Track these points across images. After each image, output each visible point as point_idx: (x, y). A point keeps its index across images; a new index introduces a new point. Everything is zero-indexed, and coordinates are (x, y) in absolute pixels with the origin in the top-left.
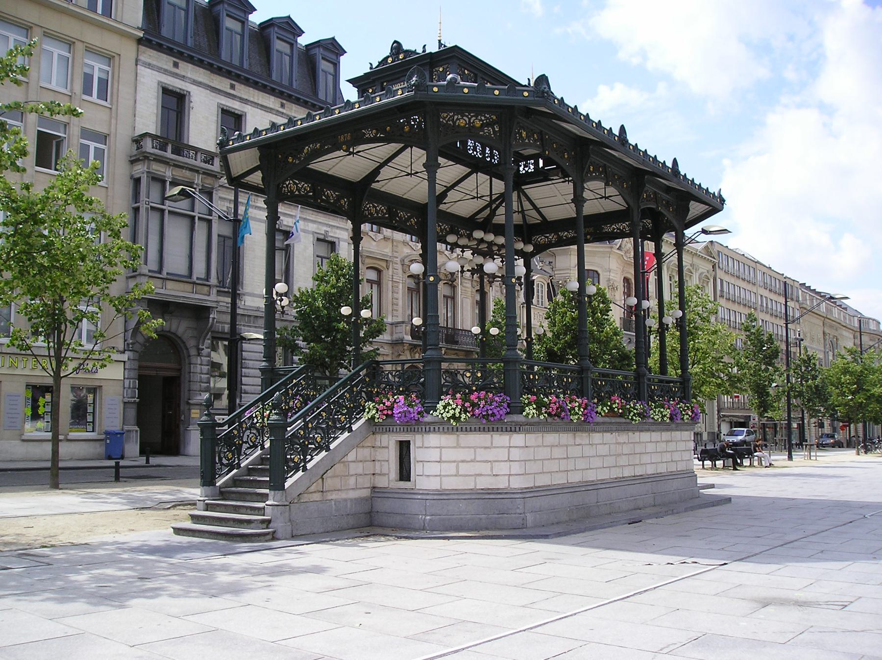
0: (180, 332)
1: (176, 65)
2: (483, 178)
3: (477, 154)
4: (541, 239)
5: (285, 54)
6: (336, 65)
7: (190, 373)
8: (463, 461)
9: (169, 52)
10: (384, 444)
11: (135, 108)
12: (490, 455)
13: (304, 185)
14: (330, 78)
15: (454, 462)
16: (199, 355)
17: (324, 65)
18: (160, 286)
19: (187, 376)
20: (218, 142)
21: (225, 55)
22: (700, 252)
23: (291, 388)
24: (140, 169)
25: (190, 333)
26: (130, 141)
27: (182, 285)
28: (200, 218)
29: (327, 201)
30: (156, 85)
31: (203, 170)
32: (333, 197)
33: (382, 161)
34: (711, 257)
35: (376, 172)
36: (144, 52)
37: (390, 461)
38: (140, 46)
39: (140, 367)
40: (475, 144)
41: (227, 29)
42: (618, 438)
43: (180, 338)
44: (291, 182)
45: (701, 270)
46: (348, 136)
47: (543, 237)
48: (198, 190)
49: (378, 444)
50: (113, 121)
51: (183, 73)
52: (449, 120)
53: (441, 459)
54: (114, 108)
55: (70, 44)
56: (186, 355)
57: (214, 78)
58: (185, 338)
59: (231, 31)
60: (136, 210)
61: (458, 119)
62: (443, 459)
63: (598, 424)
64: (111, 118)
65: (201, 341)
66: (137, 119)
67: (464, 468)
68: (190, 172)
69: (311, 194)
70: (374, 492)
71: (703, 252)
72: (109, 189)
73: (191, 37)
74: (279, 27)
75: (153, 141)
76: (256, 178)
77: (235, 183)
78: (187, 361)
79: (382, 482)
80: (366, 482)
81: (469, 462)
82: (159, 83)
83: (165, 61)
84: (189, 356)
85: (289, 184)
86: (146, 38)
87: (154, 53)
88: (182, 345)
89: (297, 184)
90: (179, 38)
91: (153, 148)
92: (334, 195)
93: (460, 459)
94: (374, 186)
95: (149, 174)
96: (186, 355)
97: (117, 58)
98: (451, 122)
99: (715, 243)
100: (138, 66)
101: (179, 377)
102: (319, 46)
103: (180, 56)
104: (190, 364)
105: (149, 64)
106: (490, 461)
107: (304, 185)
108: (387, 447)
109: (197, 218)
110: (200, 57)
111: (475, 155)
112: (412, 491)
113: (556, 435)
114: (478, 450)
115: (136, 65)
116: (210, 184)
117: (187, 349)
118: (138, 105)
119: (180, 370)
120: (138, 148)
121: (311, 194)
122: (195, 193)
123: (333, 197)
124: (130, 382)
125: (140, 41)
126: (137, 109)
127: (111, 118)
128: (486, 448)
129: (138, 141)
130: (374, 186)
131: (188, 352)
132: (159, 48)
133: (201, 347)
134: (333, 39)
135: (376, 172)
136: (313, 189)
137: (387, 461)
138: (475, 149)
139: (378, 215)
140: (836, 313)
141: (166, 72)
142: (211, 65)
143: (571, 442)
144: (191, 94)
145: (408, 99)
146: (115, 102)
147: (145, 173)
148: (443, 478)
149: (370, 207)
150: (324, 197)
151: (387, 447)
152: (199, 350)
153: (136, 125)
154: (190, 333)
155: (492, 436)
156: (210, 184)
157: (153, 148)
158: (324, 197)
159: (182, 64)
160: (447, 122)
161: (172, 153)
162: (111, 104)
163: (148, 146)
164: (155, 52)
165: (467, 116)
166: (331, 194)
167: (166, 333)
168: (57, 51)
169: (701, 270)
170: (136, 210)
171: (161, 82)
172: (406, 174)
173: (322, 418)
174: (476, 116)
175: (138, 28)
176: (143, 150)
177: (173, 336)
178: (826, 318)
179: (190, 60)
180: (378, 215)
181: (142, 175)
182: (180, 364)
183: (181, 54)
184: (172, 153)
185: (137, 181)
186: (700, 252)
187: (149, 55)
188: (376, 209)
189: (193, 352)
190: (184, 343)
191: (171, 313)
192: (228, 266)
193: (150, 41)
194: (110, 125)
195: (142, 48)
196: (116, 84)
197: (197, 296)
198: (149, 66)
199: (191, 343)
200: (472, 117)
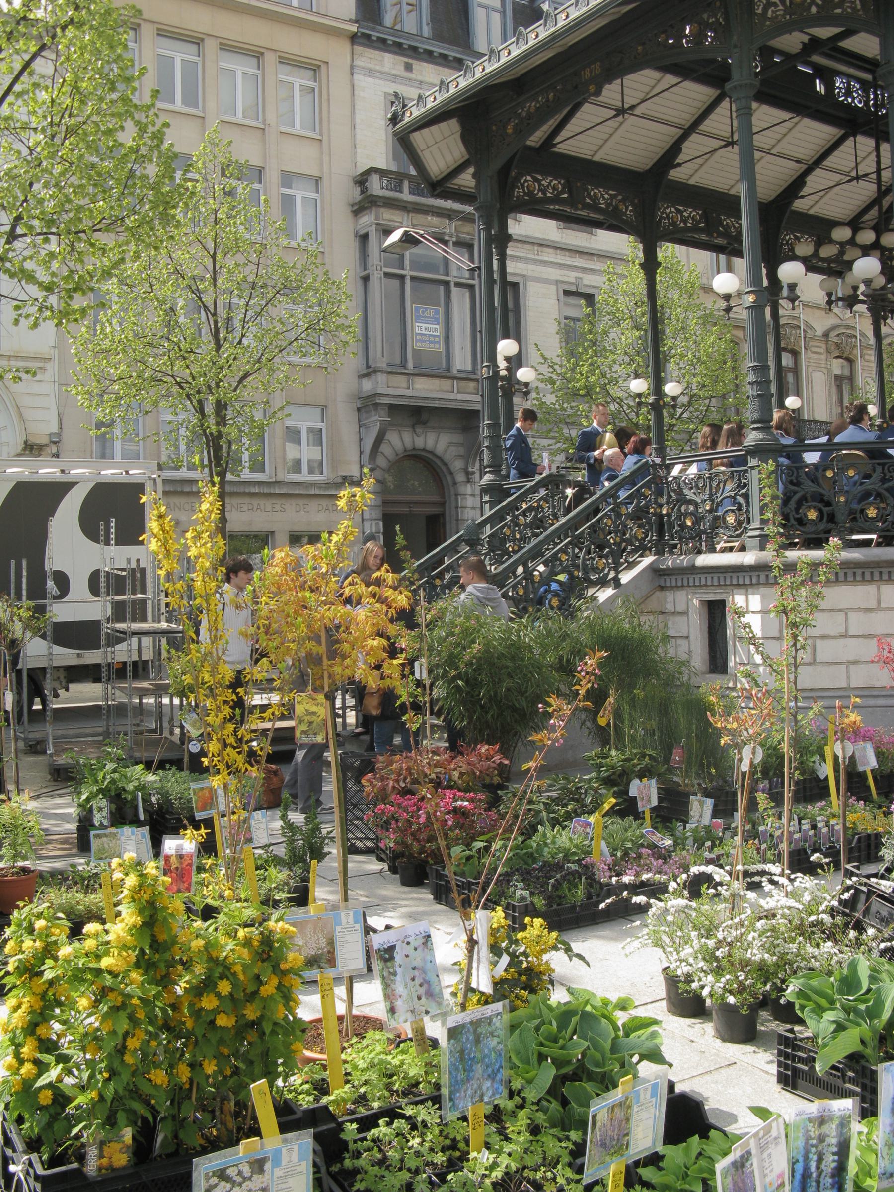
0: (440, 449)
1: (409, 67)
2: (865, 143)
3: (853, 101)
7: (457, 507)
9: (398, 48)
10: (681, 608)
11: (354, 136)
18: (405, 385)
19: (453, 512)
20: (389, 116)
24: (367, 220)
25: (453, 451)
26: (352, 184)
27: (436, 382)
28: (457, 284)
35: (675, 149)
36: (361, 55)
37: (692, 638)
38: (355, 47)
39: (385, 503)
40: (849, 85)
43: (439, 458)
44: (529, 178)
46: (597, 68)
48: (451, 244)
49: (670, 607)
50: (326, 158)
51: (420, 78)
54: (325, 141)
55: (258, 55)
56: (450, 482)
58: (447, 458)
60: (366, 279)
63: (214, 640)
64: (322, 154)
65: (471, 462)
66: (358, 150)
69: (565, 196)
72: (326, 255)
75: (381, 179)
77: (438, 190)
78: (452, 492)
83: (390, 62)
84: (455, 483)
85: (526, 181)
86: (363, 34)
87: (376, 54)
88: (444, 468)
89: (539, 181)
91: (382, 188)
94: (675, 174)
95: (380, 228)
96: (450, 482)
97: (323, 67)
100: (356, 76)
101: (443, 515)
103: (414, 52)
104: (457, 495)
105: (370, 70)
108: (685, 613)
109: (452, 284)
111: (850, 104)
113: (871, 589)
115: (352, 74)
116: (468, 234)
117: (451, 473)
118: (358, 131)
119: (443, 504)
120: (362, 192)
121: (565, 196)
122: (447, 252)
125: (354, 38)
126: (358, 137)
127: (322, 154)
128: (868, 610)
129: (362, 180)
130: (675, 174)
131: (454, 479)
132: (382, 44)
133: (470, 469)
135: (675, 149)
136: (569, 187)
137: (687, 637)
138: (848, 93)
139: (685, 224)
141: (394, 78)
146: (325, 130)
147: (374, 226)
149: (668, 212)
150: (588, 200)
151: (685, 613)
152: (468, 474)
153: (358, 159)
154: (453, 451)
155: (879, 588)
156: (468, 234)
157: (382, 188)
158: (588, 200)
159: (417, 65)
161: (410, 193)
162: (321, 134)
163: (376, 186)
164: (377, 52)
166: (603, 195)
168: (242, 67)
170: (366, 279)
172: (723, 143)
173: (561, 565)
175: (350, 21)
176: (369, 193)
177: (431, 457)
179: (429, 56)
180: (685, 224)
181: (369, 229)
182: (443, 495)
183: (414, 49)
184: (410, 193)
185: (364, 239)
187: (368, 57)
188: (682, 216)
189: (460, 478)
190: (446, 465)
191: (424, 423)
193: (368, 37)
194: (321, 164)
195: (358, 49)
196: (324, 104)
197: (460, 397)
198: (370, 72)
199: (457, 465)
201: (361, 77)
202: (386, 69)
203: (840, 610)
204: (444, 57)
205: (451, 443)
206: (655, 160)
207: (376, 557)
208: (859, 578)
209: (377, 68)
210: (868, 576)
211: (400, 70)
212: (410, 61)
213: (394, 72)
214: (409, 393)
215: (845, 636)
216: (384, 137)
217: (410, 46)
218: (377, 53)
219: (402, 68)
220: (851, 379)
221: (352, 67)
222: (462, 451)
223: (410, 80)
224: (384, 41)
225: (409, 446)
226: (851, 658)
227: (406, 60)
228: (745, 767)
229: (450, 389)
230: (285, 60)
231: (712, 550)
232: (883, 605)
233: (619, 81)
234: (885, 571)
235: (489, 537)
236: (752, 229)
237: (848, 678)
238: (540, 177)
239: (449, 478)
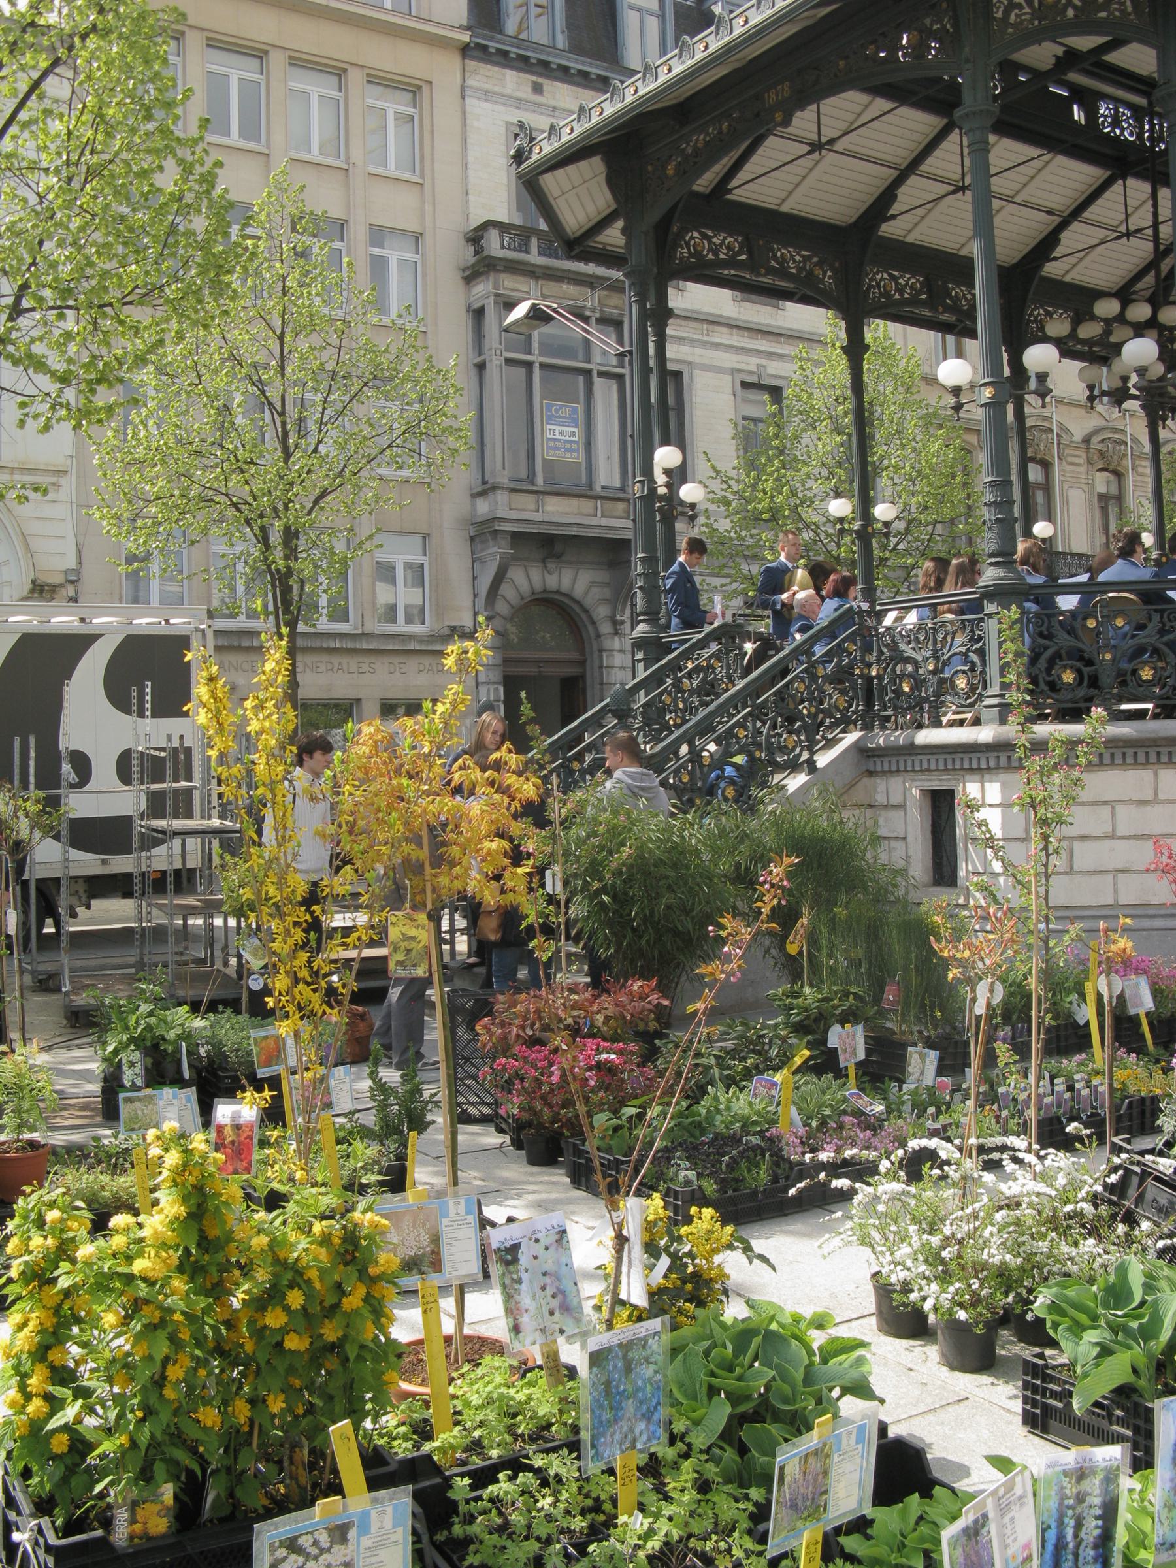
0: (579, 591)
1: (537, 89)
2: (1138, 188)
3: (1122, 133)
7: (601, 667)
9: (523, 63)
10: (896, 799)
11: (465, 178)
16: (616, 632)
18: (533, 507)
19: (596, 674)
23: (689, 676)
24: (483, 289)
25: (597, 593)
26: (463, 242)
27: (574, 502)
28: (602, 374)
29: (782, 273)
35: (888, 196)
36: (475, 72)
37: (910, 839)
38: (467, 62)
39: (506, 661)
40: (1117, 111)
43: (578, 602)
44: (696, 234)
46: (785, 89)
48: (593, 320)
49: (881, 799)
50: (428, 208)
51: (552, 103)
54: (427, 186)
55: (339, 73)
56: (592, 634)
58: (588, 602)
60: (481, 367)
64: (423, 202)
65: (619, 608)
66: (471, 198)
68: (578, 288)
69: (744, 257)
72: (429, 335)
75: (501, 236)
76: (614, 236)
77: (577, 251)
78: (595, 648)
83: (513, 82)
84: (598, 636)
85: (692, 238)
86: (477, 44)
87: (494, 71)
88: (584, 616)
91: (503, 247)
94: (888, 229)
95: (500, 300)
96: (592, 634)
97: (425, 88)
100: (468, 100)
101: (583, 677)
103: (544, 69)
104: (601, 651)
105: (487, 92)
108: (901, 807)
109: (595, 374)
111: (1118, 137)
113: (1146, 774)
115: (463, 97)
116: (616, 308)
117: (593, 623)
118: (471, 172)
119: (583, 663)
120: (477, 253)
121: (744, 257)
122: (588, 332)
125: (465, 51)
126: (472, 180)
127: (423, 202)
128: (1142, 803)
129: (476, 237)
130: (888, 229)
131: (597, 630)
132: (503, 58)
133: (618, 618)
135: (888, 196)
137: (904, 838)
138: (1116, 123)
139: (901, 294)
141: (519, 103)
146: (427, 172)
149: (879, 279)
150: (773, 263)
151: (901, 807)
152: (616, 624)
154: (597, 593)
156: (616, 308)
157: (503, 247)
158: (773, 263)
159: (548, 85)
161: (539, 254)
162: (422, 177)
163: (495, 245)
164: (496, 69)
166: (793, 257)
167: (551, 596)
168: (318, 88)
172: (951, 188)
173: (738, 743)
175: (461, 27)
176: (485, 253)
177: (566, 601)
179: (564, 74)
180: (901, 294)
181: (486, 302)
182: (582, 651)
183: (545, 64)
184: (539, 254)
185: (478, 314)
187: (485, 75)
188: (897, 284)
189: (606, 628)
190: (586, 611)
193: (484, 48)
194: (423, 216)
195: (471, 64)
196: (427, 137)
197: (605, 522)
198: (487, 95)
199: (601, 612)
201: (475, 102)
202: (508, 91)
203: (1105, 803)
204: (584, 75)
205: (593, 583)
206: (861, 211)
207: (494, 733)
208: (1129, 760)
209: (497, 89)
210: (1141, 758)
211: (526, 92)
212: (540, 80)
213: (518, 94)
214: (537, 517)
215: (1112, 836)
216: (505, 181)
217: (539, 61)
218: (496, 69)
219: (529, 89)
221: (463, 88)
222: (607, 593)
223: (540, 105)
224: (505, 54)
225: (538, 587)
226: (1120, 866)
227: (534, 78)
228: (980, 1009)
229: (591, 511)
230: (375, 79)
231: (937, 724)
232: (1161, 796)
233: (814, 107)
234: (1164, 751)
235: (643, 706)
236: (989, 301)
237: (1116, 891)
238: (710, 233)
239: (590, 628)
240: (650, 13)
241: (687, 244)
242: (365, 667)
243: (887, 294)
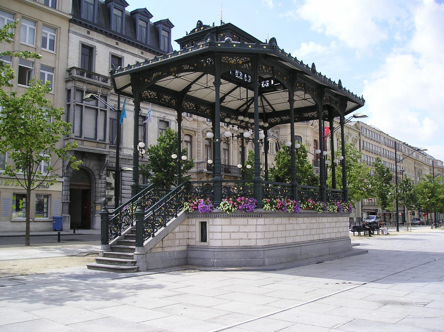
0: (91, 167)
1: (89, 33)
2: (243, 89)
3: (240, 77)
4: (272, 120)
5: (144, 27)
6: (169, 33)
7: (96, 187)
8: (233, 232)
9: (85, 26)
10: (193, 223)
11: (68, 54)
12: (247, 229)
13: (153, 93)
14: (166, 39)
15: (229, 232)
17: (163, 33)
18: (81, 144)
19: (94, 189)
21: (113, 28)
22: (352, 127)
24: (70, 85)
25: (96, 167)
26: (66, 71)
27: (91, 143)
28: (100, 110)
30: (79, 43)
31: (102, 86)
32: (168, 99)
33: (192, 81)
34: (358, 129)
35: (189, 87)
36: (72, 26)
37: (196, 232)
38: (71, 23)
39: (71, 185)
40: (239, 73)
41: (114, 14)
42: (311, 220)
43: (90, 170)
44: (147, 91)
45: (353, 136)
46: (175, 69)
47: (273, 119)
48: (100, 95)
49: (190, 223)
50: (57, 61)
51: (92, 37)
52: (226, 60)
53: (222, 231)
54: (57, 54)
55: (35, 22)
56: (94, 179)
57: (108, 39)
58: (93, 170)
59: (116, 15)
60: (69, 106)
61: (230, 60)
62: (223, 231)
63: (301, 213)
64: (56, 59)
65: (101, 172)
66: (69, 60)
67: (234, 236)
69: (157, 97)
70: (188, 247)
71: (354, 127)
72: (55, 95)
73: (96, 19)
74: (141, 14)
75: (77, 71)
77: (118, 92)
78: (94, 182)
79: (192, 243)
80: (184, 243)
81: (236, 232)
82: (80, 42)
83: (83, 31)
84: (95, 179)
85: (146, 92)
86: (74, 19)
87: (77, 27)
88: (92, 174)
90: (90, 19)
91: (77, 74)
92: (168, 98)
93: (231, 231)
94: (188, 93)
95: (75, 88)
96: (94, 179)
97: (59, 29)
98: (227, 62)
99: (360, 122)
100: (70, 33)
101: (90, 190)
102: (160, 23)
103: (91, 28)
104: (96, 183)
105: (75, 32)
106: (247, 232)
107: (153, 93)
108: (195, 225)
109: (99, 110)
110: (101, 29)
112: (207, 247)
113: (280, 219)
114: (241, 226)
115: (69, 33)
116: (106, 93)
117: (94, 176)
118: (69, 53)
119: (90, 186)
120: (69, 75)
121: (157, 97)
122: (98, 97)
123: (168, 99)
124: (65, 192)
125: (70, 21)
126: (69, 55)
127: (56, 59)
128: (245, 225)
129: (69, 71)
130: (188, 93)
131: (95, 177)
132: (80, 24)
133: (101, 174)
134: (168, 19)
135: (189, 87)
137: (195, 232)
138: (239, 75)
139: (190, 108)
140: (421, 157)
141: (83, 36)
142: (106, 33)
143: (288, 222)
144: (96, 47)
145: (205, 50)
146: (58, 52)
147: (73, 87)
148: (223, 241)
149: (186, 104)
150: (163, 99)
151: (195, 225)
152: (100, 176)
153: (69, 63)
154: (96, 167)
155: (248, 219)
156: (106, 93)
157: (77, 74)
158: (163, 99)
159: (92, 32)
160: (225, 61)
161: (87, 77)
162: (56, 52)
163: (75, 73)
164: (78, 26)
165: (235, 59)
166: (167, 98)
168: (29, 25)
169: (353, 136)
171: (81, 41)
172: (204, 87)
173: (162, 210)
174: (240, 59)
175: (70, 14)
176: (72, 75)
177: (87, 169)
178: (416, 160)
179: (96, 30)
180: (190, 108)
181: (71, 88)
182: (91, 183)
183: (91, 27)
184: (87, 77)
185: (69, 91)
186: (352, 127)
187: (75, 28)
188: (189, 105)
189: (97, 177)
190: (93, 172)
192: (115, 134)
193: (75, 21)
194: (55, 63)
195: (72, 24)
196: (58, 42)
197: (99, 149)
198: (75, 33)
199: (96, 173)
200: (238, 59)
220: (228, 150)
240: (119, 16)
241: (145, 94)
242: (71, 40)
243: (187, 108)
